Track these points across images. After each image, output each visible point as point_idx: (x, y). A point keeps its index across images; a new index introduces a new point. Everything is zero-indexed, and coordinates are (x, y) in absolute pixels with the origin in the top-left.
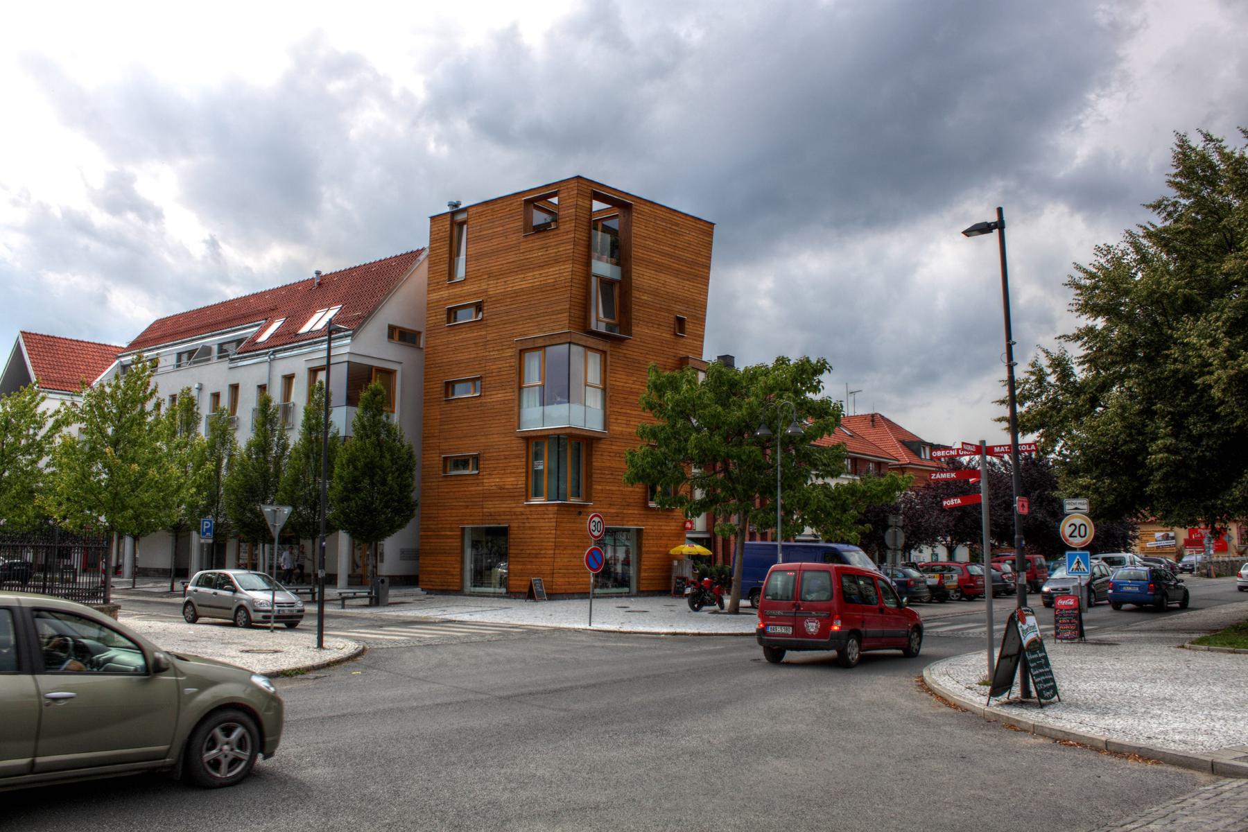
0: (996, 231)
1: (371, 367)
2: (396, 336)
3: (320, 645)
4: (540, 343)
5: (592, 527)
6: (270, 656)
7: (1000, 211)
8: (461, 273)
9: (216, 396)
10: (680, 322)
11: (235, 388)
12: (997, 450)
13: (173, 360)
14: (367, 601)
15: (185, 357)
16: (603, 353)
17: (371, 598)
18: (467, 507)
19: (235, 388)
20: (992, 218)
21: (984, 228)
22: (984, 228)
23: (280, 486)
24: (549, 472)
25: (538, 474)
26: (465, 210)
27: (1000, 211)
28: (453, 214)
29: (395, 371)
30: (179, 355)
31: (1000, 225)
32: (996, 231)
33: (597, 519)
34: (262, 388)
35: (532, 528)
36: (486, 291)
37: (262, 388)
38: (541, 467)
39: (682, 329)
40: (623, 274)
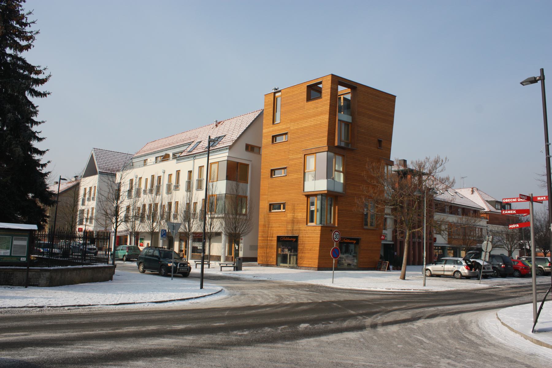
0: (540, 82)
1: (238, 163)
2: (250, 148)
3: (202, 287)
4: (314, 151)
5: (335, 237)
6: (38, 309)
7: (542, 70)
8: (278, 121)
9: (170, 175)
10: (380, 142)
11: (178, 172)
12: (539, 199)
13: (153, 159)
14: (232, 268)
15: (159, 159)
16: (343, 156)
17: (234, 267)
18: (279, 227)
19: (178, 172)
20: (538, 75)
21: (533, 81)
22: (533, 81)
23: (406, 228)
24: (317, 211)
25: (312, 212)
26: (280, 91)
27: (542, 70)
28: (275, 93)
29: (248, 165)
30: (156, 158)
31: (542, 78)
32: (540, 82)
33: (337, 233)
34: (190, 172)
35: (308, 237)
36: (289, 128)
37: (190, 172)
38: (313, 209)
39: (380, 146)
40: (353, 119)
